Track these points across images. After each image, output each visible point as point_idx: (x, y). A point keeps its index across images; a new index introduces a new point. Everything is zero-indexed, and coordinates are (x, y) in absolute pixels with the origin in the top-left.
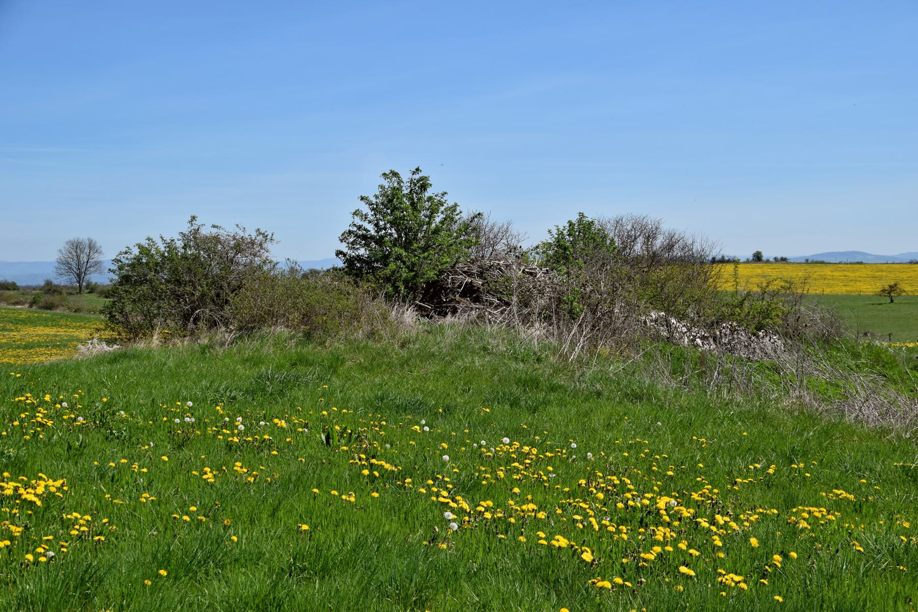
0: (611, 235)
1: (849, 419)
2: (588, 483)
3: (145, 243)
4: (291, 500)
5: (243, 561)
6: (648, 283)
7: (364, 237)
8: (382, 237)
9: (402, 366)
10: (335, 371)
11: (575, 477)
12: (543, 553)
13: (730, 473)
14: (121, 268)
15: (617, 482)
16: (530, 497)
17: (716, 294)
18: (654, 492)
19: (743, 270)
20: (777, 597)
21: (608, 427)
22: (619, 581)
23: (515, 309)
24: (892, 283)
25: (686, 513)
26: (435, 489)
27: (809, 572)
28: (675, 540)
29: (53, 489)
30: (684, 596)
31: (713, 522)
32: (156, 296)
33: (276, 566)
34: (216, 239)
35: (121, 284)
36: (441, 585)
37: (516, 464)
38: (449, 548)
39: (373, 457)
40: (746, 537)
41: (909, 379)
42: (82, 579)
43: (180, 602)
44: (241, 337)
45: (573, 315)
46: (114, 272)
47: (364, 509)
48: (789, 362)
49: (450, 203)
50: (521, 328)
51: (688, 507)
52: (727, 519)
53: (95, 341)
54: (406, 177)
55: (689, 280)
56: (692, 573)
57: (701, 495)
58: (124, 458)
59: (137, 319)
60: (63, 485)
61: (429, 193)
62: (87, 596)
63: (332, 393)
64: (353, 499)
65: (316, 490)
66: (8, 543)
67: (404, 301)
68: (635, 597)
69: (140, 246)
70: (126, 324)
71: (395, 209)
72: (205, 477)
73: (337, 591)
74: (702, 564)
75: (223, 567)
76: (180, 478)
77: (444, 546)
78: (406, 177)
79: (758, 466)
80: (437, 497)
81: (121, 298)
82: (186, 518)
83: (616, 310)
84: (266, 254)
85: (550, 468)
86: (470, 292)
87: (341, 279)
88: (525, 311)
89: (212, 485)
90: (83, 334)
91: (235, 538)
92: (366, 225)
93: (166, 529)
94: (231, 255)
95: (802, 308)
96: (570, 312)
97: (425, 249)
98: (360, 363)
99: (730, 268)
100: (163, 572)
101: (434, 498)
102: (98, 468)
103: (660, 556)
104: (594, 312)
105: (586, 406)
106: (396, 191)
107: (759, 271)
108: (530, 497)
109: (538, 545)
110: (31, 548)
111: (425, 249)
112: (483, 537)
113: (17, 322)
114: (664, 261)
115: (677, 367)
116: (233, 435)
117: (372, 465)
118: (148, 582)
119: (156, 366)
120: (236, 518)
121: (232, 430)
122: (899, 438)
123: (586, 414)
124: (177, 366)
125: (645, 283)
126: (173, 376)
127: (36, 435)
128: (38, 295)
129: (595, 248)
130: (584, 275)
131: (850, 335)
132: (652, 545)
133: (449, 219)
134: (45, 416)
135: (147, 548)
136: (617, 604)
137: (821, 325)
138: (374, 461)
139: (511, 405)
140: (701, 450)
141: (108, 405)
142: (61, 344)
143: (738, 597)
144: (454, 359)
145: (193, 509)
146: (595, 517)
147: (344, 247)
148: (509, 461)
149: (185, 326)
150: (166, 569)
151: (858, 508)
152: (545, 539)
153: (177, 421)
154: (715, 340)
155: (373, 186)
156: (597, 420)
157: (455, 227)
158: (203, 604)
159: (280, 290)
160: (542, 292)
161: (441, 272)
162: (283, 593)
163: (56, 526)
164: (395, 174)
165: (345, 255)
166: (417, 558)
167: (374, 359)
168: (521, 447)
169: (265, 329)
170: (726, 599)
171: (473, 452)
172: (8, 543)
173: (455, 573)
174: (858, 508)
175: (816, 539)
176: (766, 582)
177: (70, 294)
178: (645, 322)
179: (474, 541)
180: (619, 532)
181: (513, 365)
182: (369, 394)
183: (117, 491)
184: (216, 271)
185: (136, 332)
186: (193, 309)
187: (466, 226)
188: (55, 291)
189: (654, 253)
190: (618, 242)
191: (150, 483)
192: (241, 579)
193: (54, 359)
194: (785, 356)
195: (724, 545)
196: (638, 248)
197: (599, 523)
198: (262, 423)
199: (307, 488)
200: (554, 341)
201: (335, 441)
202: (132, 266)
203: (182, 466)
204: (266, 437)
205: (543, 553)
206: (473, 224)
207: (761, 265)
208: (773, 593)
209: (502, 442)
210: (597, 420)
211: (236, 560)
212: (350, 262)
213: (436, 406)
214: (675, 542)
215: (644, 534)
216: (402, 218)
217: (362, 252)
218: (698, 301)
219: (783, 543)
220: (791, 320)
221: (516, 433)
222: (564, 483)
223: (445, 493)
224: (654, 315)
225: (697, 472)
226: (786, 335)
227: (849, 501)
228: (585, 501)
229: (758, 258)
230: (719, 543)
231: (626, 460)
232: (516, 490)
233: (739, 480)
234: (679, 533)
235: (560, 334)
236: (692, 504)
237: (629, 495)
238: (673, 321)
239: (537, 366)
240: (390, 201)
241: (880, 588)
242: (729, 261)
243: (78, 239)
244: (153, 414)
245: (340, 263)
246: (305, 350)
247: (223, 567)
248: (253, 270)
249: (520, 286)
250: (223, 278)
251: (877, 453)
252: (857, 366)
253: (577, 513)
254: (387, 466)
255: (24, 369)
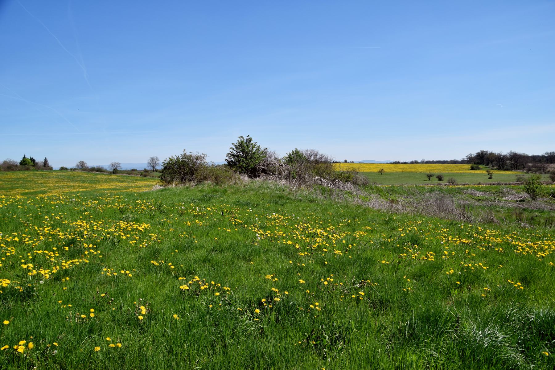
0: (304, 155)
1: (370, 207)
2: (298, 226)
3: (171, 157)
4: (212, 231)
5: (199, 248)
6: (315, 168)
7: (233, 155)
8: (238, 155)
9: (244, 192)
10: (225, 194)
11: (294, 224)
12: (285, 246)
13: (338, 222)
14: (164, 165)
15: (306, 225)
16: (281, 230)
17: (334, 172)
18: (317, 228)
19: (342, 165)
20: (350, 257)
21: (304, 210)
22: (306, 253)
23: (277, 176)
24: (382, 169)
25: (325, 234)
26: (254, 228)
27: (359, 249)
28: (322, 241)
29: (146, 227)
30: (325, 257)
31: (333, 236)
32: (174, 173)
33: (208, 249)
34: (191, 156)
35: (164, 169)
36: (256, 255)
37: (277, 221)
38: (258, 244)
39: (236, 219)
40: (342, 240)
41: (386, 195)
42: (155, 252)
43: (182, 259)
44: (198, 184)
45: (293, 178)
46: (162, 166)
47: (233, 233)
48: (354, 190)
49: (258, 145)
50: (278, 181)
51: (326, 232)
52: (337, 235)
53: (157, 185)
54: (245, 138)
55: (327, 167)
56: (327, 251)
57: (330, 229)
58: (165, 218)
59: (169, 179)
60: (149, 226)
61: (252, 142)
62: (156, 257)
63: (224, 200)
64: (230, 231)
65: (219, 228)
66: (135, 241)
67: (245, 174)
68: (311, 258)
69: (170, 158)
70: (166, 181)
71: (242, 147)
72: (188, 224)
73: (226, 257)
74: (329, 248)
75: (193, 250)
76: (181, 224)
77: (256, 244)
78: (245, 138)
79: (346, 220)
80: (254, 230)
81: (164, 173)
82: (183, 236)
83: (306, 176)
84: (205, 160)
85: (287, 222)
86: (264, 171)
87: (226, 167)
88: (280, 176)
89: (190, 227)
90: (154, 183)
91: (196, 242)
92: (234, 152)
93: (177, 239)
94: (195, 160)
95: (358, 176)
96: (293, 177)
97: (251, 158)
98: (232, 192)
99: (338, 164)
100: (177, 251)
101: (253, 231)
102: (158, 221)
103: (318, 246)
104: (300, 177)
105: (297, 204)
106: (242, 142)
107: (346, 165)
108: (281, 230)
109: (283, 244)
110: (141, 243)
111: (251, 158)
112: (267, 241)
113: (137, 180)
114: (319, 162)
115: (323, 191)
116: (195, 212)
117: (235, 221)
118: (173, 253)
119: (174, 192)
120: (197, 236)
121: (195, 211)
122: (383, 212)
123: (297, 206)
124: (180, 193)
125: (314, 168)
126: (179, 195)
127: (141, 212)
128: (142, 173)
129: (300, 158)
130: (297, 166)
131: (371, 183)
132: (316, 243)
133: (258, 150)
134: (144, 206)
135: (172, 244)
136: (306, 260)
137: (363, 181)
138: (236, 220)
139: (276, 204)
140: (330, 216)
141: (161, 203)
142: (149, 186)
143: (339, 257)
144: (259, 190)
145: (185, 233)
146: (300, 235)
147: (227, 158)
148: (275, 220)
149: (182, 181)
150: (177, 250)
151: (372, 231)
152: (285, 242)
153: (180, 208)
154: (334, 185)
155: (236, 140)
156: (301, 208)
157: (259, 152)
158: (188, 260)
159: (209, 170)
160: (284, 171)
161: (255, 165)
162: (210, 257)
163: (147, 237)
164: (242, 137)
165: (227, 160)
166: (248, 247)
167: (236, 190)
168: (279, 216)
169: (205, 182)
170: (336, 258)
171: (265, 217)
172: (135, 241)
173: (259, 252)
174: (372, 231)
175: (361, 240)
176: (347, 252)
177: (151, 172)
178: (314, 180)
179: (265, 243)
180: (306, 239)
181: (276, 192)
182: (234, 200)
183: (163, 228)
184: (191, 165)
185: (169, 183)
186: (185, 176)
187: (263, 152)
188: (147, 171)
189: (317, 160)
190: (306, 157)
191: (172, 226)
192: (199, 253)
193: (146, 191)
194: (353, 189)
195: (336, 243)
196: (312, 158)
197: (301, 237)
198: (204, 209)
199: (217, 228)
200: (288, 185)
201: (225, 214)
202: (167, 164)
203: (181, 221)
204: (205, 213)
205: (285, 246)
206: (265, 151)
207: (396, 169)
208: (349, 255)
209: (273, 214)
210: (301, 208)
211: (197, 248)
212: (229, 162)
213: (254, 204)
214: (322, 242)
215: (313, 240)
216: (244, 150)
217: (233, 159)
218: (329, 174)
219: (352, 242)
220: (355, 179)
221: (277, 212)
222: (291, 226)
223: (256, 229)
224: (317, 178)
225: (329, 222)
226: (353, 183)
227: (370, 230)
228: (297, 231)
229: (346, 161)
230: (334, 242)
231: (309, 219)
232: (277, 228)
233: (340, 224)
234: (323, 240)
235: (290, 183)
236: (327, 231)
237: (309, 229)
238: (322, 179)
239: (283, 192)
240: (241, 145)
241: (377, 253)
242: (338, 162)
243: (471, 154)
244: (173, 206)
245: (226, 163)
246: (216, 188)
247: (193, 250)
248: (201, 165)
249: (278, 169)
250: (193, 167)
251: (377, 216)
252: (373, 192)
253: (294, 234)
254: (240, 221)
255: (138, 194)
